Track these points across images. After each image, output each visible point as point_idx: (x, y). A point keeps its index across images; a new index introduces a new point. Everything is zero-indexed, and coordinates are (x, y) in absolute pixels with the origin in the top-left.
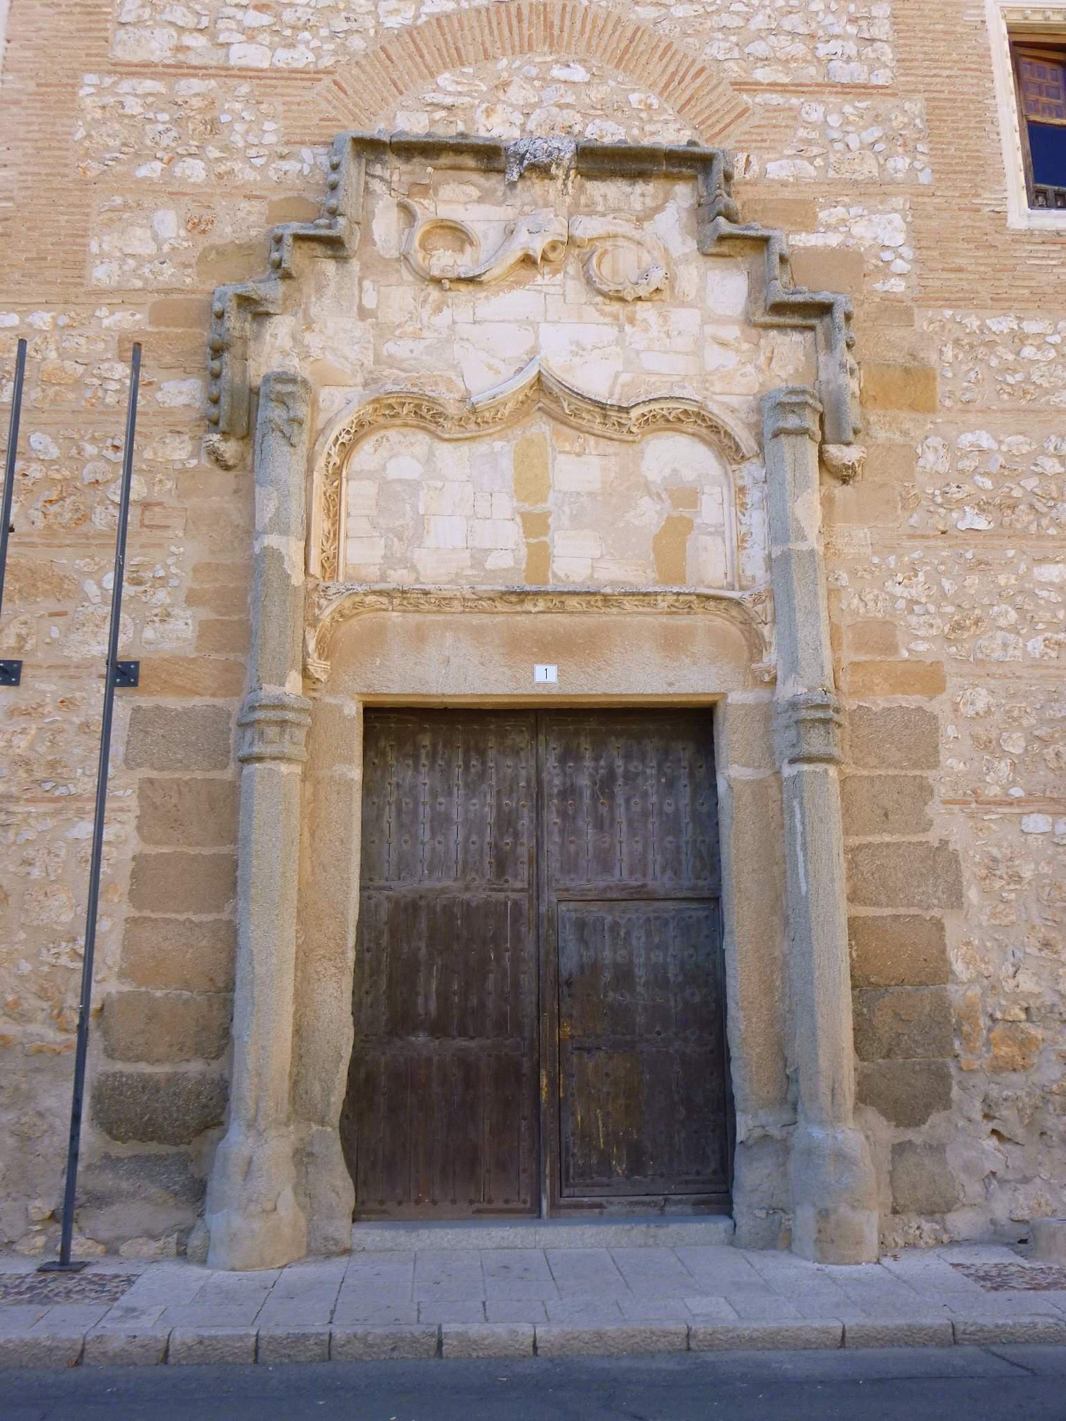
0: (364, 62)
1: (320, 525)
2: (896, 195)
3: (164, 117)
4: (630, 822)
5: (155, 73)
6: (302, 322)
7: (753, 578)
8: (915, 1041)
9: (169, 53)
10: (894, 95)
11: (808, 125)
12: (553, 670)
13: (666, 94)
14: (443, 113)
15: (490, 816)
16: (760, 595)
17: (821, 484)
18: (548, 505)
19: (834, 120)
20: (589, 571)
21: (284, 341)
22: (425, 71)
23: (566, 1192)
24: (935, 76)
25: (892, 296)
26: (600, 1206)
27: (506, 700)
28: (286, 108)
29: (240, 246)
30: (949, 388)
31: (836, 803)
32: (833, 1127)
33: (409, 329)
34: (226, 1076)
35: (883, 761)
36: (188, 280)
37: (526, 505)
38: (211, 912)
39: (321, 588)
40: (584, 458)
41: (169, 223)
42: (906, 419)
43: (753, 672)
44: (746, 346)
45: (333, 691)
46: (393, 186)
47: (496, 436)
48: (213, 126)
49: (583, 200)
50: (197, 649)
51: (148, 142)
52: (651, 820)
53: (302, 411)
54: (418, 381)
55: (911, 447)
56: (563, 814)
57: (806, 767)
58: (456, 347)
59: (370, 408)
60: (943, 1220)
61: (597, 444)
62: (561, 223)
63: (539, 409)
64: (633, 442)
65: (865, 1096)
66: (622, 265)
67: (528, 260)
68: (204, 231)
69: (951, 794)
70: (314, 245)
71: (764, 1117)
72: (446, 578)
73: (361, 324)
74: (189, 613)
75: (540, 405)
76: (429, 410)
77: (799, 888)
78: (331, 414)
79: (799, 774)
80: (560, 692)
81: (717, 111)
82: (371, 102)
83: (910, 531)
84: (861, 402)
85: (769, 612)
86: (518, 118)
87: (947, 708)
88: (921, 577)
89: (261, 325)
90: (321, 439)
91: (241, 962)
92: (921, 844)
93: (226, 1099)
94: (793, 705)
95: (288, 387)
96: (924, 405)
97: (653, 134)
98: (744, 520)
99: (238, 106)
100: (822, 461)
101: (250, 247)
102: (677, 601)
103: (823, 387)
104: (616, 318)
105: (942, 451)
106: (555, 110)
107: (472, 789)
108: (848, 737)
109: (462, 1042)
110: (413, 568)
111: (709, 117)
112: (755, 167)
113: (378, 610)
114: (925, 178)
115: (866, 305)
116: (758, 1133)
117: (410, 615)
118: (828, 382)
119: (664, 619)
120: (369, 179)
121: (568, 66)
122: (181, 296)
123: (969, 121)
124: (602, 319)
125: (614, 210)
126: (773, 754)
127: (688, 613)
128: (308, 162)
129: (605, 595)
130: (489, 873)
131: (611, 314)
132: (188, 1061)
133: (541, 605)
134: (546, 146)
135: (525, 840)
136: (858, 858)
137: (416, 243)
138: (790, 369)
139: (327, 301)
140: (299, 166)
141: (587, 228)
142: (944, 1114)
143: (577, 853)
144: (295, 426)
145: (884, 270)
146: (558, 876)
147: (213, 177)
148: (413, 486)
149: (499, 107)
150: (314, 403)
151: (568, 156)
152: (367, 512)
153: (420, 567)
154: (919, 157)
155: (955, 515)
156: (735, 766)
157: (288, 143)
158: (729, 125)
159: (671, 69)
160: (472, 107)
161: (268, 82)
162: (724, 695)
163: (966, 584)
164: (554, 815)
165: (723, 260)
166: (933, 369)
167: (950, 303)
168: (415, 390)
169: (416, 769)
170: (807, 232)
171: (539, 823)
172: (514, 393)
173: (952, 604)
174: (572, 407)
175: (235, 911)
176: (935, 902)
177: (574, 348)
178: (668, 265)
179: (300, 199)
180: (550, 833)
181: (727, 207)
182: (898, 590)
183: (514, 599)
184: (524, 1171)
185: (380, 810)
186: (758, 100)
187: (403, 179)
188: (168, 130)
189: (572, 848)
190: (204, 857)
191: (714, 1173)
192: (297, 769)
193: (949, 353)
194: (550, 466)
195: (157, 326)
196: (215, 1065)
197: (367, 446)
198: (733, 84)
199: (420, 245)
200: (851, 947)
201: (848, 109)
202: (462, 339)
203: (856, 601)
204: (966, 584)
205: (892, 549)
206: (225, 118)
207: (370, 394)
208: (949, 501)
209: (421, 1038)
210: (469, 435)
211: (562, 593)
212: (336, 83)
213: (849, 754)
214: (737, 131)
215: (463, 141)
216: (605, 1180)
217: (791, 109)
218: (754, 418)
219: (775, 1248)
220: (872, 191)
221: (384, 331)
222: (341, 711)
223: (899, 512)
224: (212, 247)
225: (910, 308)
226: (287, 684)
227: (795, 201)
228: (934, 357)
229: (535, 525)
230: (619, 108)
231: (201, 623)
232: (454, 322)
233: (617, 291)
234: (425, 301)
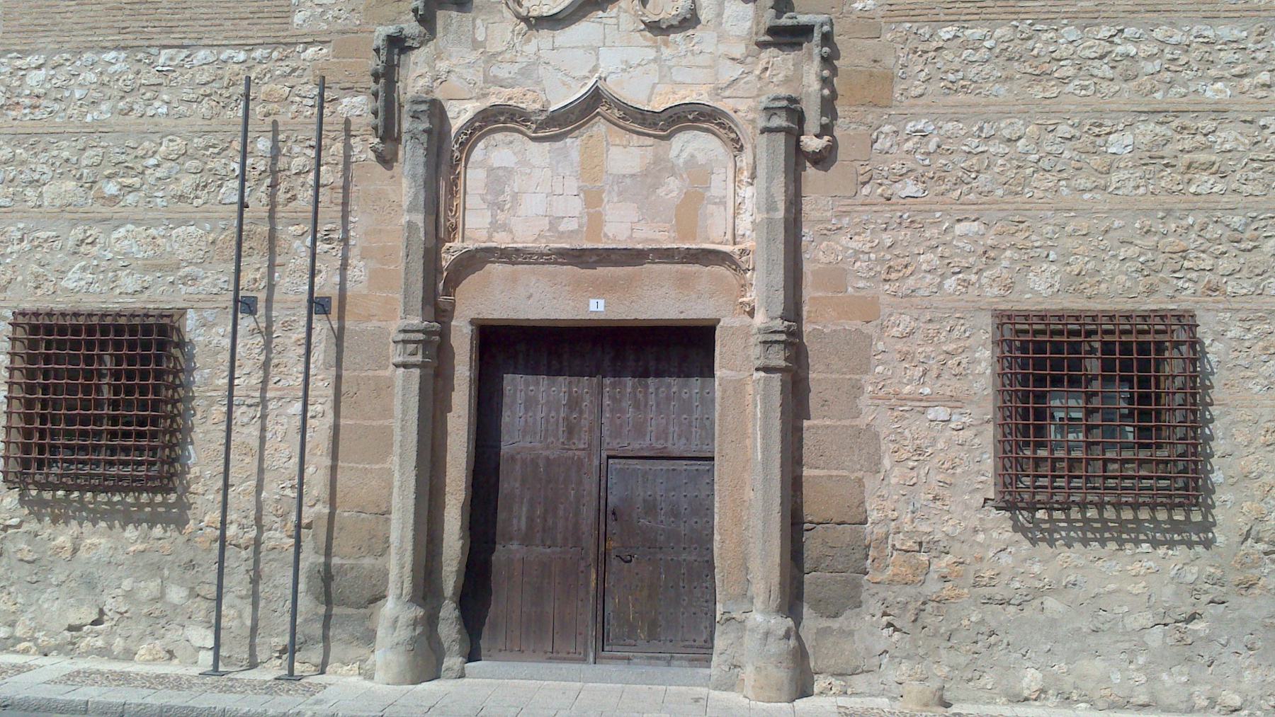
4: (658, 405)
23: (606, 648)
56: (613, 398)
110: (511, 232)
135: (586, 416)
139: (451, 37)
143: (621, 425)
148: (509, 171)
162: (719, 321)
189: (618, 422)
216: (633, 642)
229: (592, 198)
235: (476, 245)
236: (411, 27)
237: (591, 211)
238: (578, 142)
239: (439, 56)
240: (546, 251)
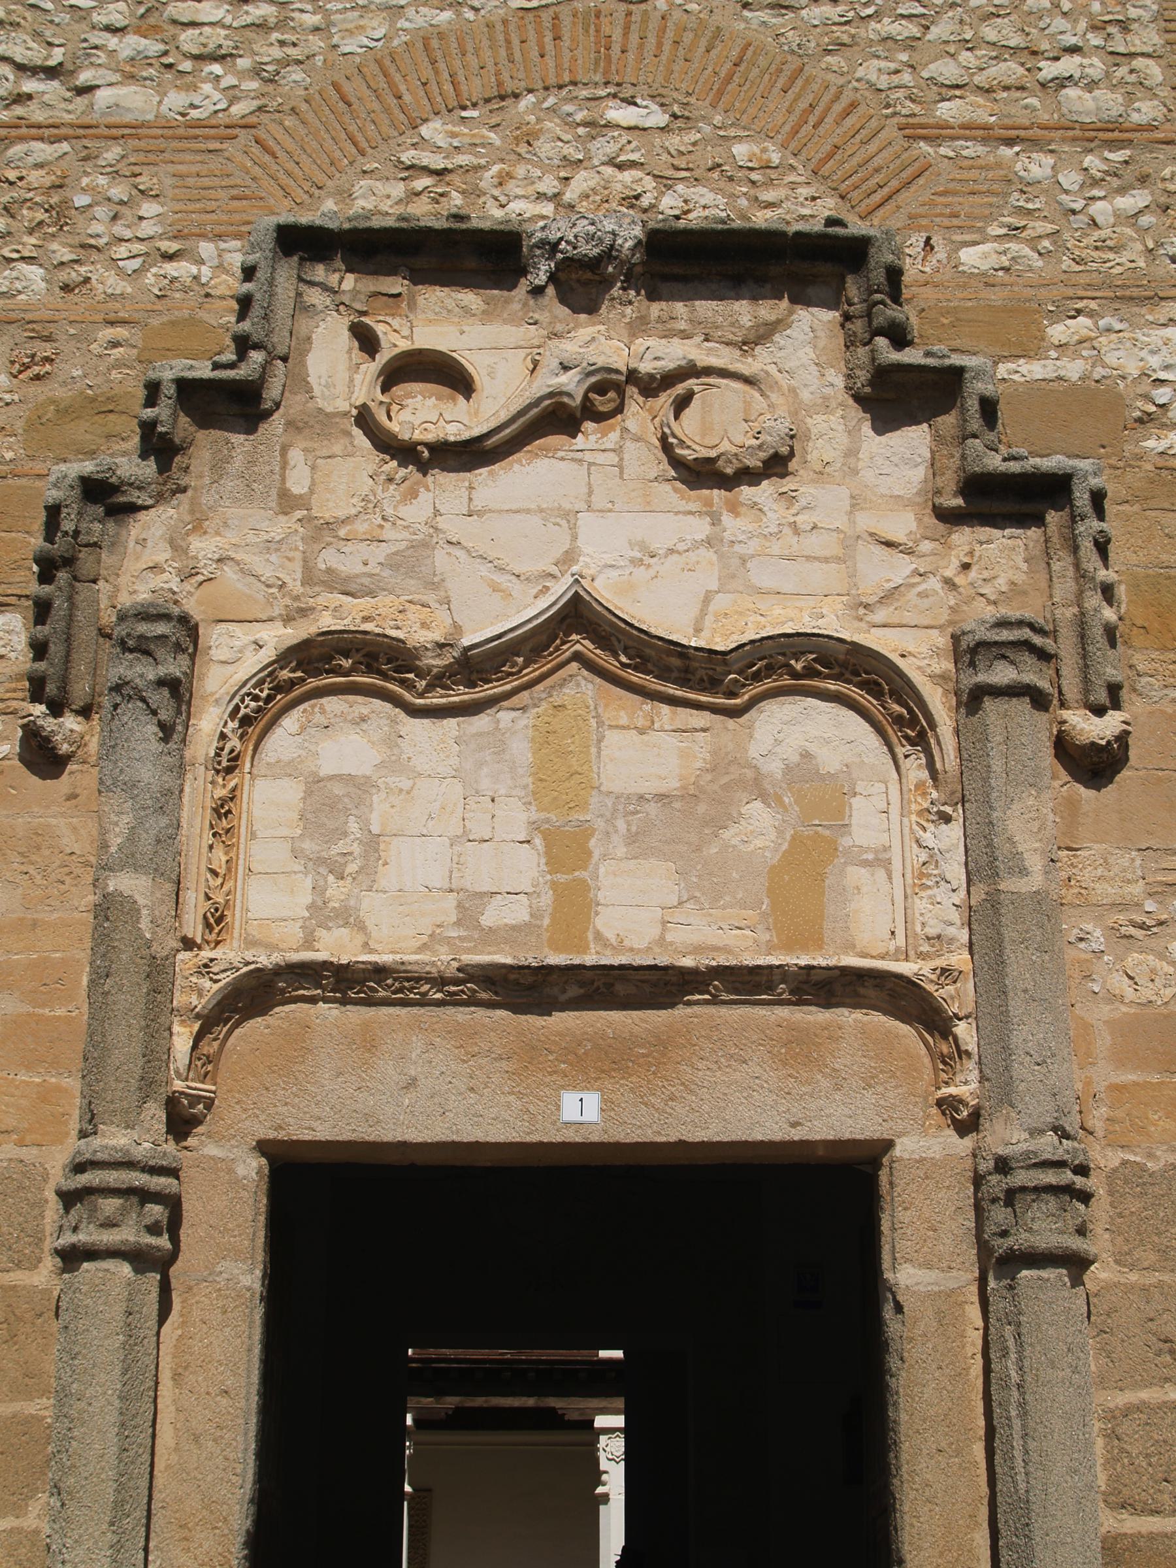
19: (1070, 179)
40: (652, 737)
48: (61, 215)
66: (719, 424)
68: (38, 377)
106: (609, 171)
110: (361, 927)
120: (303, 287)
139: (229, 484)
148: (361, 786)
152: (285, 832)
153: (369, 924)
162: (889, 1145)
194: (593, 750)
229: (566, 849)
232: (437, 513)
235: (277, 958)
236: (130, 465)
237: (562, 878)
238: (525, 720)
239: (198, 526)
240: (451, 971)
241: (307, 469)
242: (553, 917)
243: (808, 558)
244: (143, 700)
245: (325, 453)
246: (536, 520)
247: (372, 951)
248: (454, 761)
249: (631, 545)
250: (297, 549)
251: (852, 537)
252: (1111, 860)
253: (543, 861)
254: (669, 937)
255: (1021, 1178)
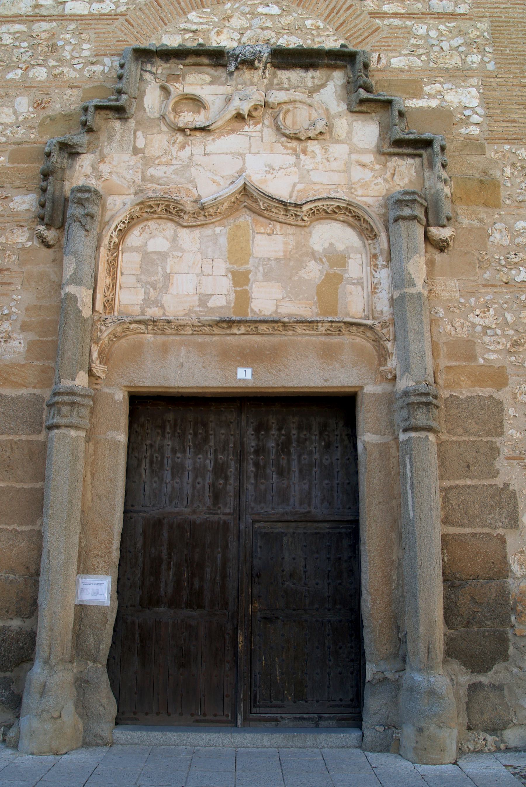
0: (144, 8)
1: (104, 280)
2: (472, 77)
3: (25, 44)
4: (301, 471)
5: (21, 20)
6: (98, 157)
7: (382, 311)
8: (485, 616)
9: (30, 9)
10: (470, 19)
11: (416, 37)
12: (249, 371)
13: (328, 20)
14: (191, 35)
15: (210, 465)
16: (385, 322)
17: (426, 252)
18: (249, 266)
19: (433, 34)
20: (274, 308)
21: (88, 170)
22: (181, 11)
23: (254, 710)
24: (496, 8)
25: (471, 137)
26: (276, 720)
27: (219, 390)
28: (96, 36)
29: (65, 115)
30: (508, 193)
31: (434, 458)
32: (428, 673)
33: (164, 160)
34: (35, 630)
35: (466, 431)
36: (32, 136)
37: (235, 266)
38: (28, 525)
39: (102, 319)
40: (273, 237)
41: (23, 104)
42: (482, 212)
43: (381, 372)
44: (377, 167)
45: (108, 385)
46: (158, 76)
47: (217, 223)
48: (53, 48)
49: (275, 81)
50: (26, 358)
51: (15, 59)
52: (315, 469)
53: (93, 209)
54: (168, 191)
55: (484, 229)
56: (256, 465)
57: (413, 434)
58: (193, 169)
59: (138, 208)
60: (501, 734)
61: (281, 227)
62: (260, 94)
63: (245, 206)
64: (305, 226)
65: (452, 651)
66: (299, 119)
67: (239, 117)
68: (44, 108)
69: (511, 453)
70: (108, 112)
71: (383, 666)
72: (184, 313)
73: (134, 157)
74: (22, 336)
75: (246, 204)
76: (174, 208)
77: (409, 514)
78: (114, 212)
79: (410, 439)
80: (254, 385)
81: (360, 29)
82: (148, 30)
83: (484, 282)
84: (452, 201)
85: (391, 334)
86: (236, 36)
87: (509, 396)
88: (492, 312)
89: (73, 160)
90: (107, 227)
91: (44, 556)
92: (491, 486)
93: (34, 644)
94: (406, 393)
95: (87, 195)
96: (492, 203)
97: (320, 43)
98: (376, 275)
99: (68, 36)
100: (427, 238)
101: (70, 115)
102: (331, 326)
103: (427, 192)
104: (295, 150)
105: (505, 232)
106: (259, 31)
107: (199, 448)
108: (443, 416)
109: (187, 612)
110: (162, 307)
111: (354, 33)
112: (384, 61)
113: (138, 333)
114: (491, 66)
115: (454, 142)
116: (380, 676)
117: (159, 336)
118: (430, 189)
119: (323, 339)
120: (143, 72)
121: (268, 6)
122: (27, 146)
123: (518, 34)
124: (285, 151)
125: (295, 88)
126: (394, 426)
127: (339, 335)
128: (108, 65)
129: (284, 323)
130: (208, 500)
131: (291, 148)
132: (12, 619)
133: (243, 330)
134: (252, 50)
135: (231, 481)
136: (450, 495)
137: (170, 109)
138: (406, 180)
139: (114, 145)
140: (102, 68)
141: (277, 96)
142: (503, 664)
144: (89, 219)
145: (466, 121)
146: (253, 504)
147: (51, 77)
148: (163, 256)
149: (225, 30)
150: (104, 207)
151: (266, 55)
152: (134, 272)
153: (166, 306)
154: (487, 54)
155: (513, 272)
156: (369, 434)
157: (96, 55)
158: (367, 37)
159: (331, 6)
160: (208, 30)
161: (87, 22)
162: (362, 388)
163: (521, 316)
164: (251, 465)
165: (363, 115)
166: (498, 181)
167: (508, 141)
168: (166, 196)
169: (163, 436)
170: (417, 98)
171: (240, 471)
172: (228, 197)
173: (512, 329)
174: (266, 205)
175: (41, 525)
176: (500, 524)
177: (267, 169)
178: (328, 118)
179: (102, 87)
180: (248, 478)
181: (365, 82)
182: (477, 320)
183: (225, 325)
184: (227, 696)
185: (140, 461)
186: (385, 23)
187: (164, 72)
188: (27, 51)
189: (262, 487)
190: (25, 490)
191: (352, 700)
192: (83, 434)
193: (508, 171)
194: (251, 242)
195: (13, 163)
196: (28, 621)
197: (136, 232)
198: (369, 14)
199: (173, 110)
200: (443, 553)
201: (442, 27)
202: (197, 165)
203: (449, 327)
204: (521, 316)
205: (472, 294)
206: (60, 43)
207: (138, 199)
208: (509, 263)
209: (161, 610)
210: (199, 223)
211: (256, 322)
212: (127, 20)
213: (444, 426)
214: (373, 40)
215: (201, 48)
216: (279, 703)
217: (406, 27)
218: (382, 211)
219: (388, 751)
220: (458, 75)
221: (148, 162)
222: (113, 398)
223: (477, 270)
224: (49, 117)
225: (483, 144)
226: (76, 379)
227: (410, 81)
228: (499, 174)
229: (240, 279)
230: (299, 29)
231: (29, 343)
232: (192, 155)
233: (295, 134)
234: (174, 143)
237: (238, 289)
239: (102, 160)
241: (143, 139)
242: (235, 303)
243: (332, 171)
244: (80, 222)
245: (150, 133)
246: (230, 157)
247: (166, 316)
248: (198, 246)
249: (266, 166)
250: (139, 168)
251: (351, 161)
252: (447, 283)
253: (232, 282)
254: (279, 311)
255: (413, 399)
